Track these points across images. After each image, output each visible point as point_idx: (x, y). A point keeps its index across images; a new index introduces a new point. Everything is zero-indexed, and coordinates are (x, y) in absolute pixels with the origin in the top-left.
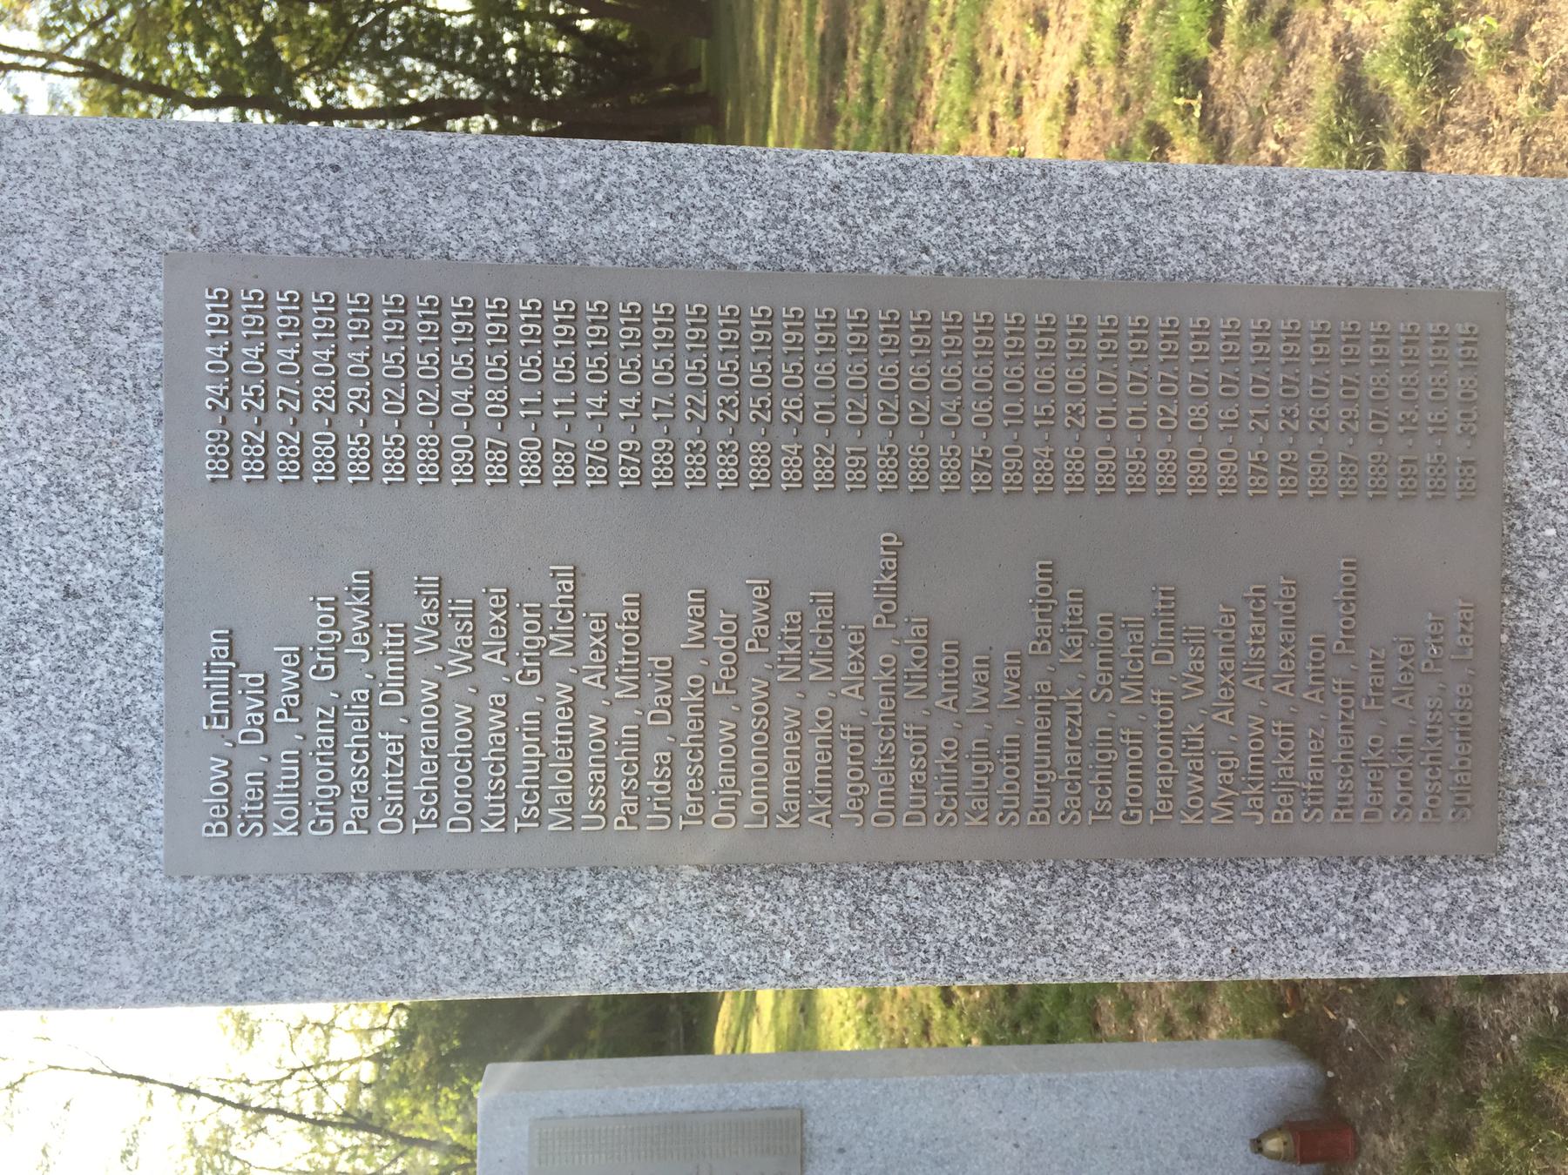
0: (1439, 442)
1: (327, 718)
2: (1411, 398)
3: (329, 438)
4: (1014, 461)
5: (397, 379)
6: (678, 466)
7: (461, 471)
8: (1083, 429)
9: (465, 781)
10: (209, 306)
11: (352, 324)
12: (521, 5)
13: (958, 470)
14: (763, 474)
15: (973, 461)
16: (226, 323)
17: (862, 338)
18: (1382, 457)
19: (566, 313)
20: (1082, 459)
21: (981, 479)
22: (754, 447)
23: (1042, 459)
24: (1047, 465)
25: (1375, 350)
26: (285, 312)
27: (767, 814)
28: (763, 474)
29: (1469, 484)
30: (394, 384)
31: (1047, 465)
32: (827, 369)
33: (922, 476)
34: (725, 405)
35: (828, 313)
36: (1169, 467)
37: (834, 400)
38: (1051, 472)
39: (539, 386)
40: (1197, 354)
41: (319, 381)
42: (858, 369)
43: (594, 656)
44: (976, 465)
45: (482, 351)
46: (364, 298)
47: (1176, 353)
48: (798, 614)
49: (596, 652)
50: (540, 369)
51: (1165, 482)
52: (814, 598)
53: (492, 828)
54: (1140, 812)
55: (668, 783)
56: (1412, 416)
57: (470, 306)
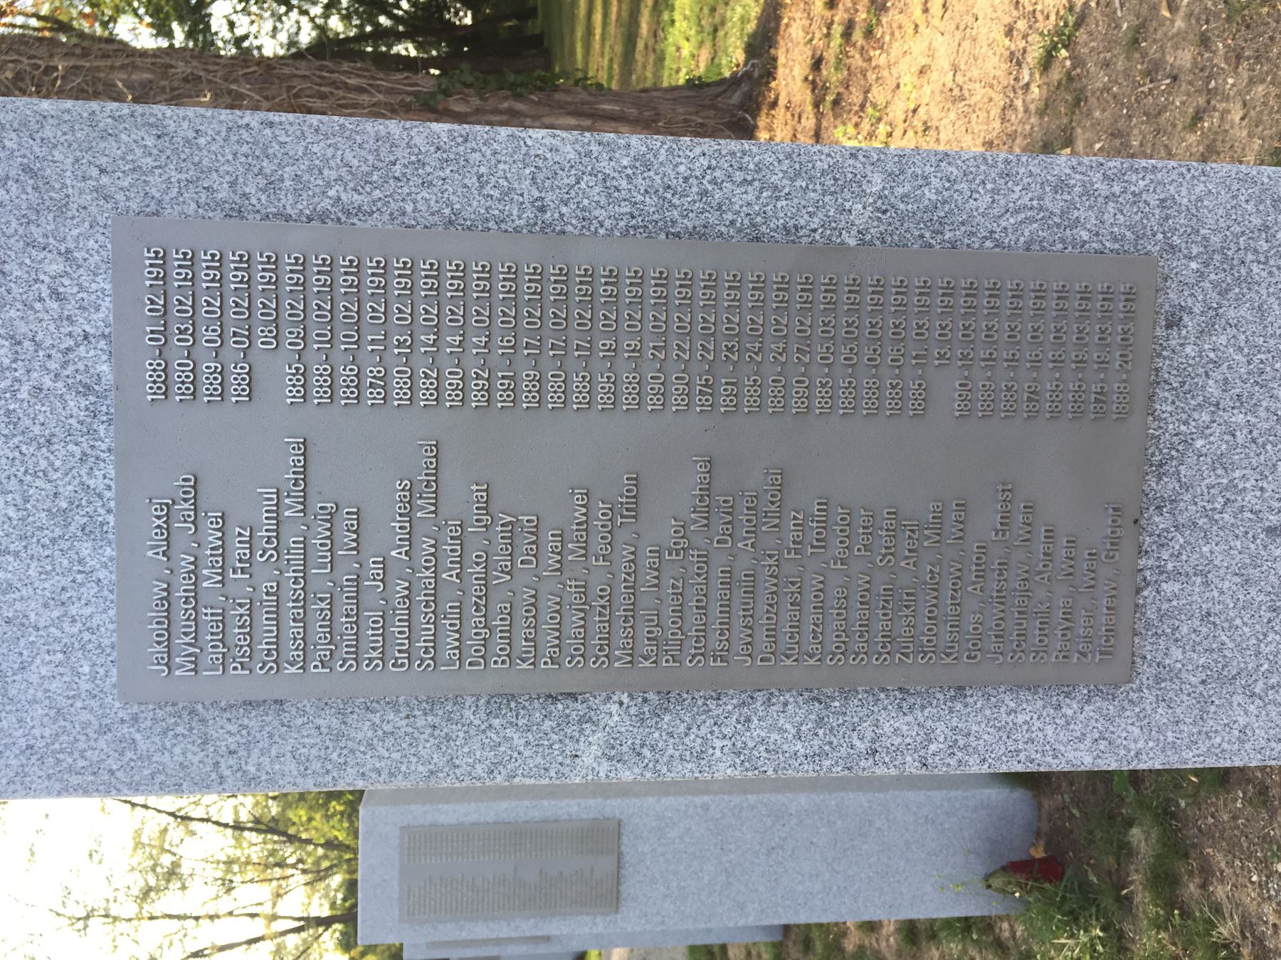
1: (630, 582)
2: (969, 339)
3: (188, 365)
4: (801, 390)
10: (147, 262)
14: (159, 388)
15: (698, 388)
16: (245, 279)
17: (662, 292)
18: (990, 386)
19: (483, 272)
25: (965, 302)
26: (180, 267)
28: (850, 403)
30: (240, 324)
35: (535, 268)
36: (920, 394)
38: (900, 399)
39: (563, 333)
41: (180, 320)
43: (156, 534)
46: (353, 261)
47: (951, 307)
48: (940, 504)
49: (158, 531)
53: (525, 666)
54: (979, 653)
55: (432, 626)
57: (245, 259)
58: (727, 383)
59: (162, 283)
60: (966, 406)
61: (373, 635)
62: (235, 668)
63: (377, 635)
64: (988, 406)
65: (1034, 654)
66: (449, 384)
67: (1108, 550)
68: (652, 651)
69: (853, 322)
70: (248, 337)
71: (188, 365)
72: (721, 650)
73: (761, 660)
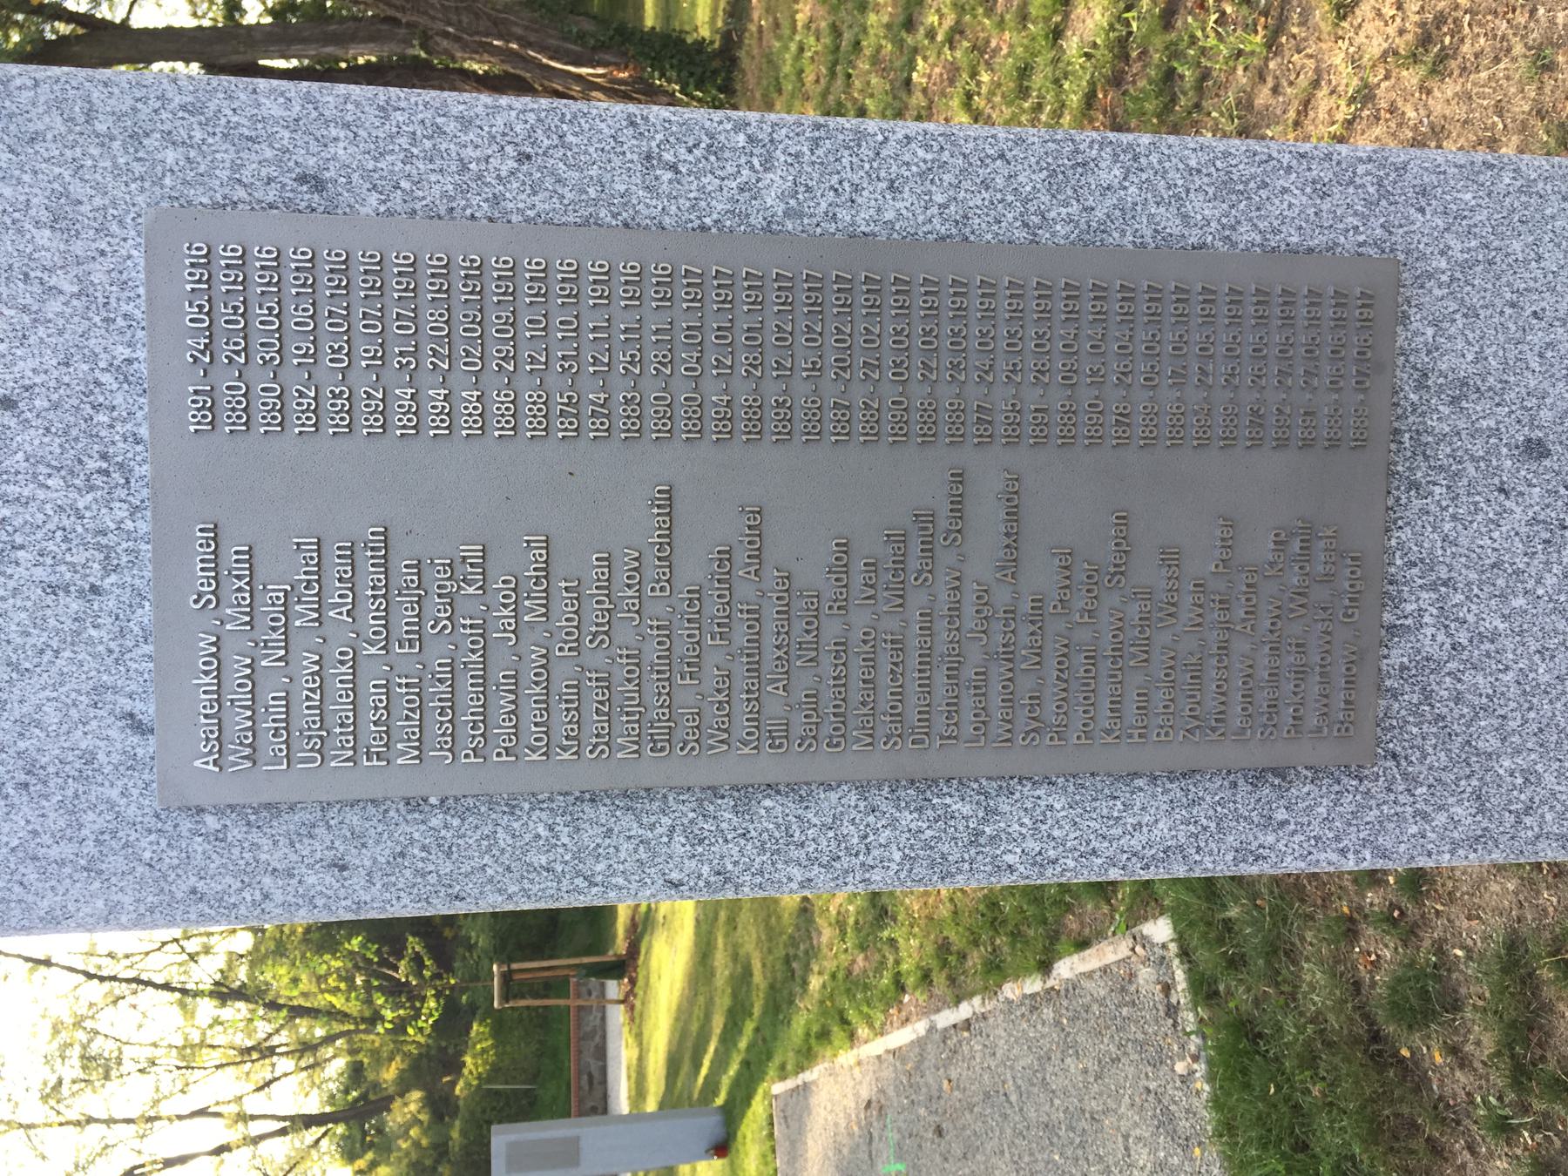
0: (1178, 394)
3: (239, 388)
6: (487, 416)
7: (234, 419)
13: (699, 419)
14: (239, 417)
22: (530, 396)
23: (470, 402)
24: (475, 408)
25: (1121, 307)
28: (539, 423)
29: (1178, 432)
32: (304, 310)
34: (435, 353)
37: (576, 349)
40: (627, 299)
41: (367, 338)
42: (304, 310)
45: (489, 308)
50: (208, 314)
52: (298, 544)
56: (1099, 370)
59: (206, 286)
60: (1041, 431)
62: (499, 754)
64: (754, 426)
65: (1338, 726)
67: (1346, 607)
69: (932, 330)
71: (239, 388)
72: (1058, 726)
73: (913, 743)
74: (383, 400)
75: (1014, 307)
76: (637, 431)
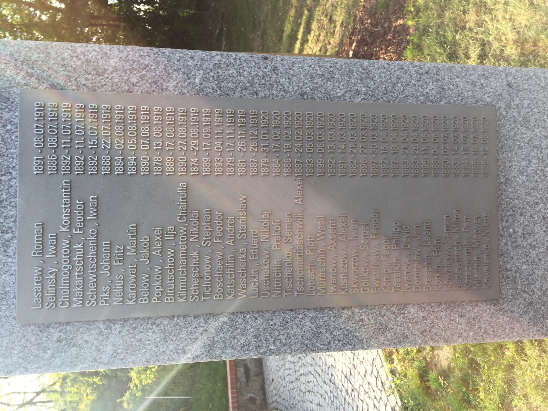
5: (208, 138)
8: (302, 153)
9: (134, 286)
11: (117, 117)
12: (139, 1)
13: (257, 167)
15: (262, 164)
20: (290, 163)
21: (206, 170)
24: (121, 163)
27: (258, 293)
29: (437, 171)
31: (278, 165)
33: (300, 170)
38: (356, 168)
44: (228, 165)
51: (242, 171)
55: (122, 281)
58: (37, 159)
59: (83, 120)
61: (169, 283)
62: (102, 303)
63: (171, 283)
66: (143, 164)
68: (232, 291)
70: (149, 144)
74: (97, 161)
75: (395, 126)
76: (197, 172)
